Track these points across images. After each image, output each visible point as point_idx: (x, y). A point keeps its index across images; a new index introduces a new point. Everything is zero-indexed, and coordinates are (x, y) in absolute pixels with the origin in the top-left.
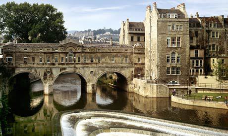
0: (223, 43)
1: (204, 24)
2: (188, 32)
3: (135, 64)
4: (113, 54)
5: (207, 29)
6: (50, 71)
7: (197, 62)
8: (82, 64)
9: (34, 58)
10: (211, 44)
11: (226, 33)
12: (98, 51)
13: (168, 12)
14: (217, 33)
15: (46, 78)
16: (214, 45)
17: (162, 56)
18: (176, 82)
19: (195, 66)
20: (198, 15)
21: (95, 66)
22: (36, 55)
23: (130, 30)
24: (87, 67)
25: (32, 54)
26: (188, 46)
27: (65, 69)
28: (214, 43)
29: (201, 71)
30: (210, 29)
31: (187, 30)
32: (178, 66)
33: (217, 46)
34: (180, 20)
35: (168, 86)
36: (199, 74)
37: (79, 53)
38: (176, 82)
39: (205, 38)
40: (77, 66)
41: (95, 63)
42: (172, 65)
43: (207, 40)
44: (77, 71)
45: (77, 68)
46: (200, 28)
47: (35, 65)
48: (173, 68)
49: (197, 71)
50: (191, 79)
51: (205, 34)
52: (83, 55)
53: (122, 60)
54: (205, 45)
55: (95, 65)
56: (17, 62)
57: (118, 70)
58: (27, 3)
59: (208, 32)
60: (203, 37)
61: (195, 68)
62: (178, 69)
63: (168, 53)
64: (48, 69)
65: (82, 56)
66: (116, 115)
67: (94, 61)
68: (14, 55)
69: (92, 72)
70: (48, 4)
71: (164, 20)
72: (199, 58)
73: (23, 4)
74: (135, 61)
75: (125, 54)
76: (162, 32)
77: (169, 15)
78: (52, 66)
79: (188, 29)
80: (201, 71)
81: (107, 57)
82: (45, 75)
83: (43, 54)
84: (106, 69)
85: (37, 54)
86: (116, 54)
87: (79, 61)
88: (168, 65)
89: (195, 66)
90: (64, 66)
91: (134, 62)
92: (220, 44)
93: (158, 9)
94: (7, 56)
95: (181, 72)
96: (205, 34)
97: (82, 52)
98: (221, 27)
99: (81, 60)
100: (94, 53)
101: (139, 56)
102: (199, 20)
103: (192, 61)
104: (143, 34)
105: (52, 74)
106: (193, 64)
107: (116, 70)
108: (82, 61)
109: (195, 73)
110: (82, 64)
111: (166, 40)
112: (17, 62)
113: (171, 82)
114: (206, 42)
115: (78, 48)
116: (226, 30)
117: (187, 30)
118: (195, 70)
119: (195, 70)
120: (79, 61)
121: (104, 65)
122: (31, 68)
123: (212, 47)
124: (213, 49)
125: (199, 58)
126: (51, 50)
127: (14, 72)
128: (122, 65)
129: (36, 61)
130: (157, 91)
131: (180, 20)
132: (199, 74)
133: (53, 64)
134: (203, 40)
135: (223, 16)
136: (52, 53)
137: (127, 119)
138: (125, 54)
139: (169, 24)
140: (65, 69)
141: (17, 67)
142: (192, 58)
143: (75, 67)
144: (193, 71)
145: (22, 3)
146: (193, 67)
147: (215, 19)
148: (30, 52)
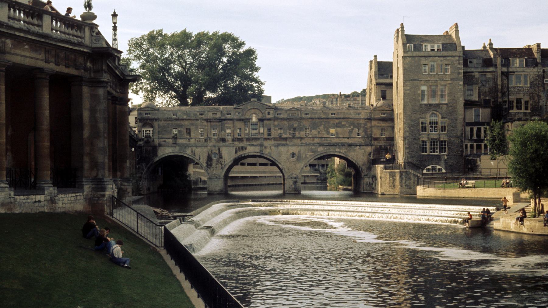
0: (539, 97)
1: (499, 60)
2: (462, 75)
3: (376, 139)
4: (332, 122)
5: (505, 69)
6: (217, 152)
7: (479, 130)
8: (275, 139)
9: (190, 129)
10: (512, 98)
11: (544, 77)
12: (304, 116)
13: (426, 41)
14: (526, 76)
15: (211, 165)
16: (520, 99)
17: (411, 120)
18: (438, 167)
19: (475, 137)
20: (491, 44)
21: (300, 143)
22: (192, 125)
23: (379, 78)
24: (283, 145)
25: (186, 123)
26: (461, 101)
27: (243, 148)
28: (519, 96)
29: (486, 146)
30: (511, 70)
31: (459, 73)
32: (443, 138)
33: (526, 103)
34: (446, 53)
35: (423, 174)
36: (483, 152)
37: (269, 119)
38: (438, 167)
39: (500, 87)
40: (266, 143)
41: (298, 138)
42: (431, 137)
43: (506, 90)
44: (267, 152)
45: (266, 147)
46: (491, 69)
47: (192, 141)
48: (433, 142)
49: (479, 147)
50: (469, 162)
51: (499, 79)
52: (276, 123)
53: (351, 132)
54: (500, 100)
55: (298, 141)
56: (160, 136)
57: (342, 151)
58: (187, 31)
59: (506, 75)
60: (496, 84)
61: (476, 141)
62: (442, 143)
63: (423, 115)
64: (213, 149)
65: (275, 126)
66: (33, 155)
67: (297, 135)
68: (156, 124)
69: (293, 154)
70: (202, 31)
71: (414, 55)
72: (483, 124)
73: (178, 36)
74: (375, 134)
75: (355, 121)
76: (412, 77)
77: (426, 46)
78: (221, 144)
79: (462, 71)
80: (486, 146)
81: (322, 128)
82: (209, 159)
83: (205, 123)
84: (320, 149)
85: (195, 122)
86: (337, 121)
87: (269, 135)
88: (424, 137)
89: (475, 137)
90: (241, 144)
91: (373, 136)
92: (532, 98)
93: (406, 35)
94: (144, 126)
95: (449, 148)
96: (499, 79)
97: (275, 119)
98: (536, 64)
99: (272, 131)
100: (296, 120)
101: (383, 124)
102: (491, 54)
103: (468, 129)
104: (391, 85)
105: (221, 158)
106: (472, 135)
107: (337, 150)
108: (275, 133)
109: (475, 152)
110: (275, 139)
111: (420, 92)
112: (160, 136)
113: (430, 167)
114: (503, 94)
115: (268, 110)
116: (544, 71)
117: (459, 73)
118: (475, 144)
119: (475, 144)
120: (269, 135)
121: (316, 140)
122: (186, 146)
123: (515, 104)
124: (519, 108)
125: (483, 124)
126: (218, 116)
127: (156, 154)
128: (350, 141)
129: (193, 135)
130: (401, 182)
131: (446, 53)
132: (483, 152)
133: (223, 140)
134: (497, 91)
135: (539, 45)
136: (220, 120)
137: (255, 206)
138: (355, 121)
139: (423, 61)
140: (243, 148)
141: (160, 145)
142: (468, 124)
143: (261, 145)
144: (472, 146)
145: (99, 29)
146: (471, 140)
147: (526, 52)
148: (183, 120)
